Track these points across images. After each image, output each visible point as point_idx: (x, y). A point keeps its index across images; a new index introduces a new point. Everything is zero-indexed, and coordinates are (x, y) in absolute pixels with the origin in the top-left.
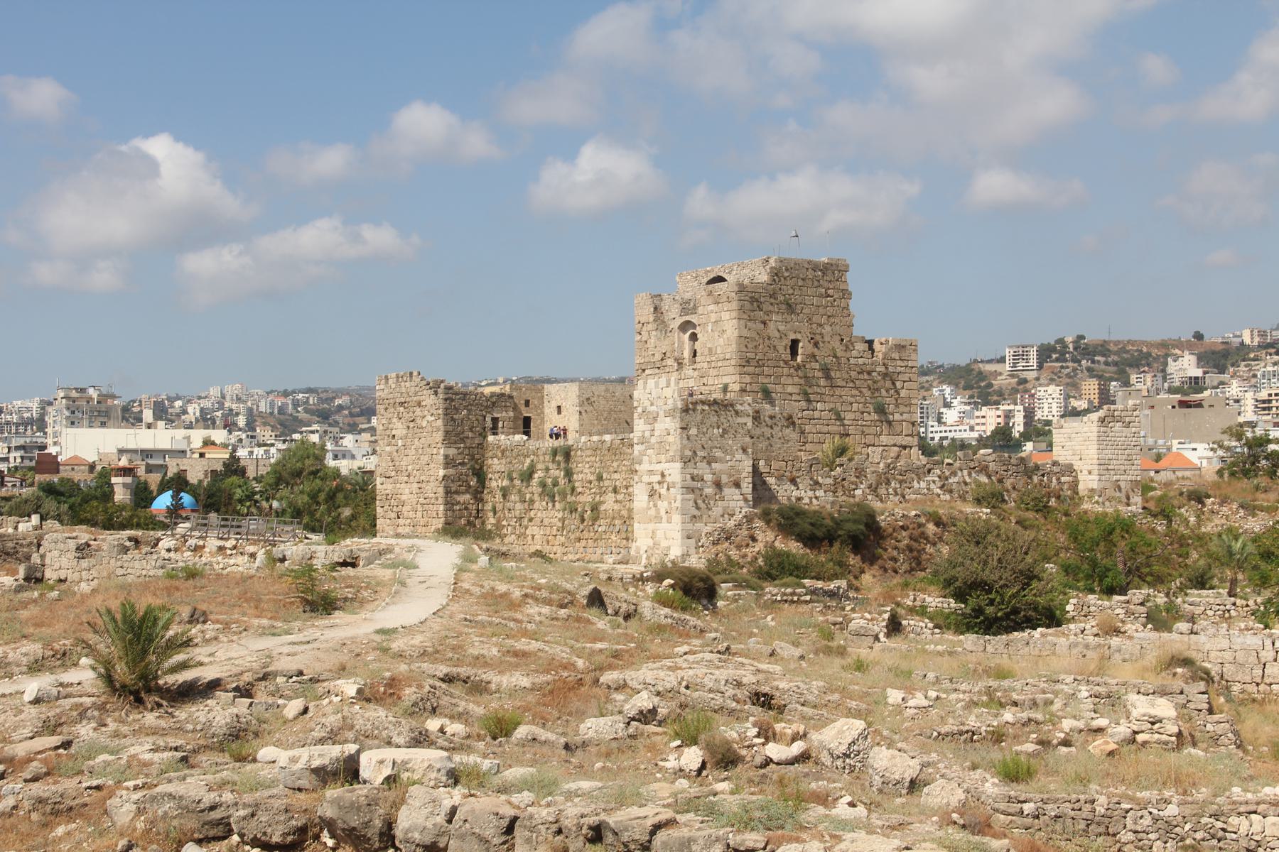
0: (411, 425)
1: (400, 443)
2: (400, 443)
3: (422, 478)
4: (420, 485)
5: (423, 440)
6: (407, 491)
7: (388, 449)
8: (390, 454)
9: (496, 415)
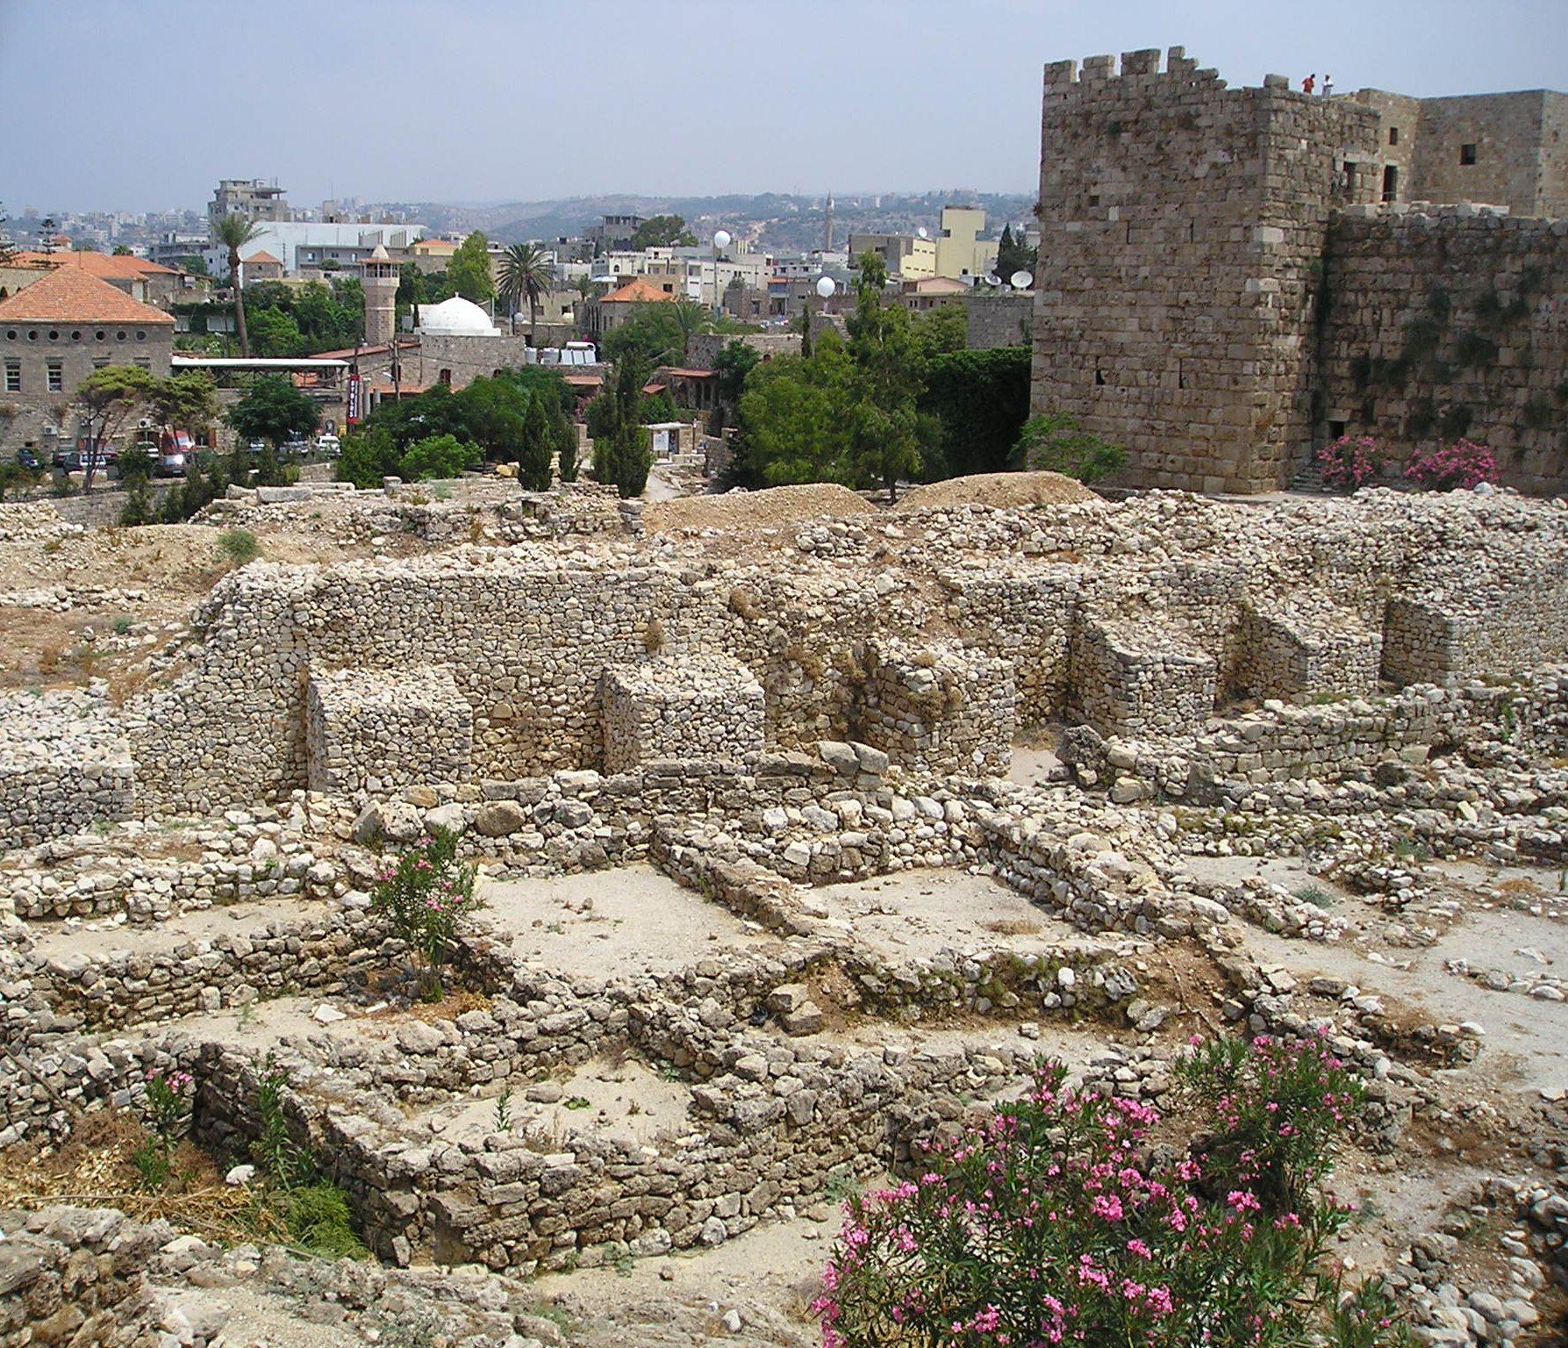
0: (1154, 174)
1: (1114, 214)
2: (1114, 214)
3: (1184, 296)
4: (1177, 313)
5: (1195, 210)
6: (1133, 324)
7: (1073, 227)
8: (1079, 238)
9: (1351, 158)
